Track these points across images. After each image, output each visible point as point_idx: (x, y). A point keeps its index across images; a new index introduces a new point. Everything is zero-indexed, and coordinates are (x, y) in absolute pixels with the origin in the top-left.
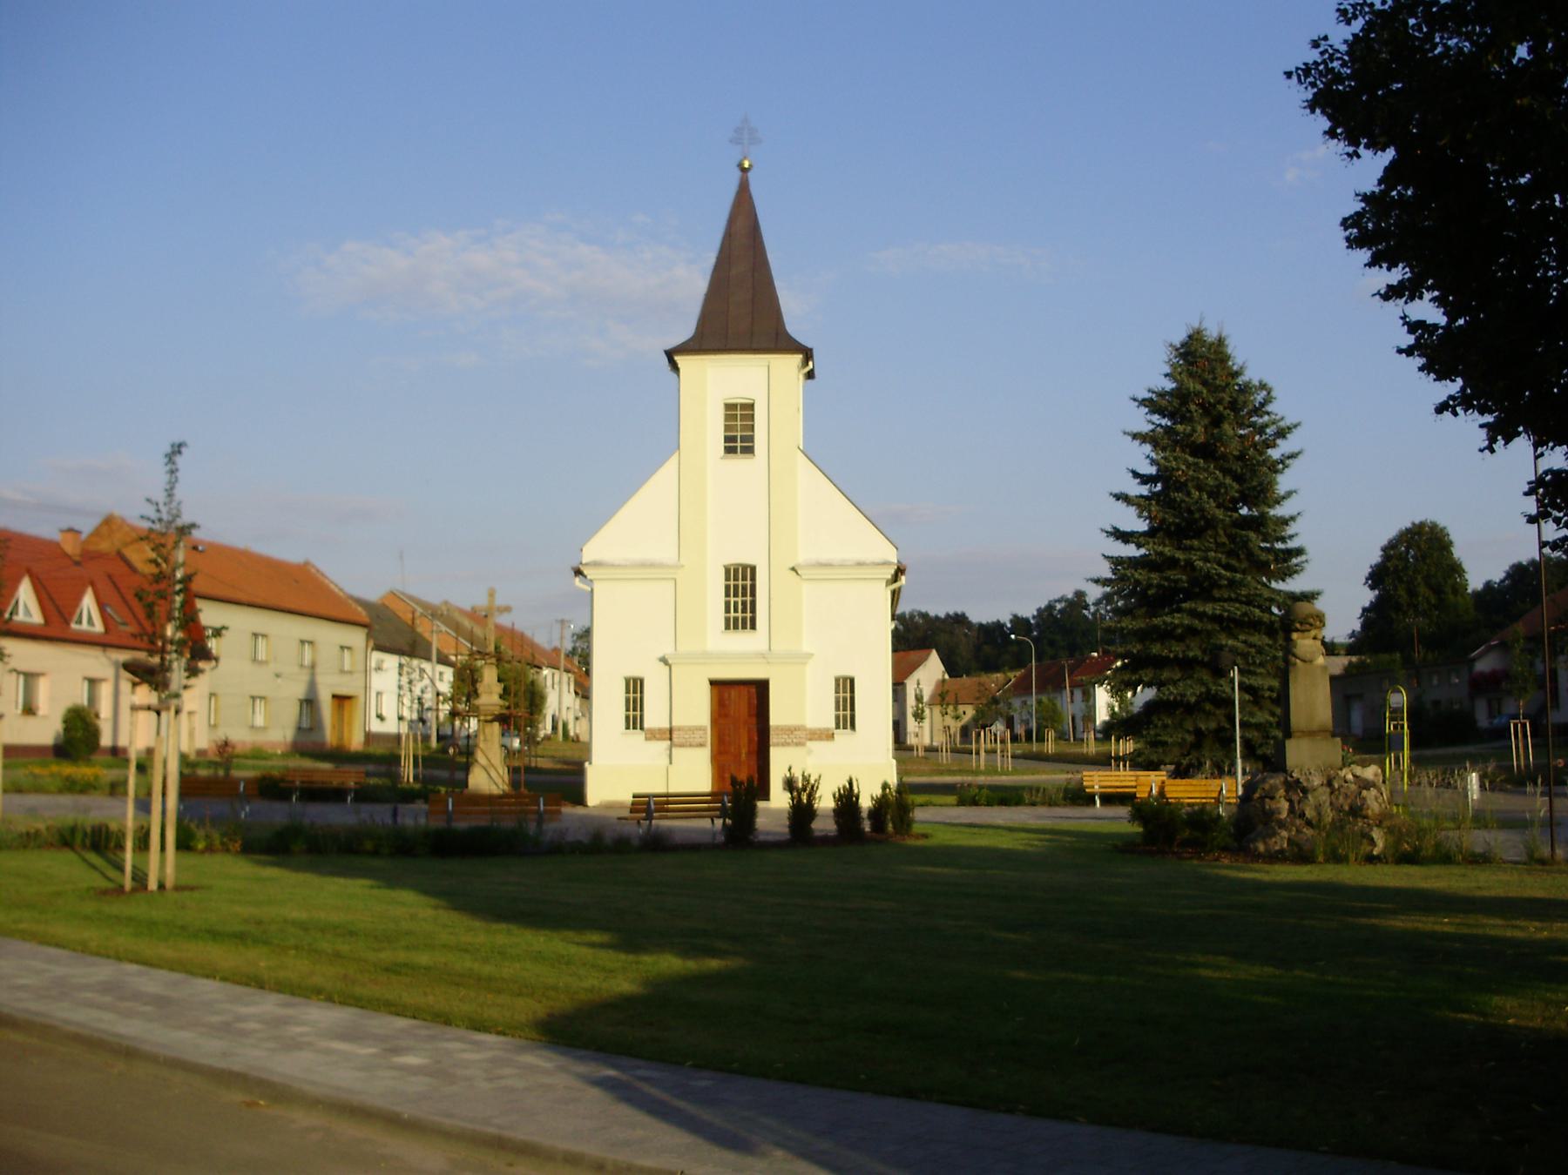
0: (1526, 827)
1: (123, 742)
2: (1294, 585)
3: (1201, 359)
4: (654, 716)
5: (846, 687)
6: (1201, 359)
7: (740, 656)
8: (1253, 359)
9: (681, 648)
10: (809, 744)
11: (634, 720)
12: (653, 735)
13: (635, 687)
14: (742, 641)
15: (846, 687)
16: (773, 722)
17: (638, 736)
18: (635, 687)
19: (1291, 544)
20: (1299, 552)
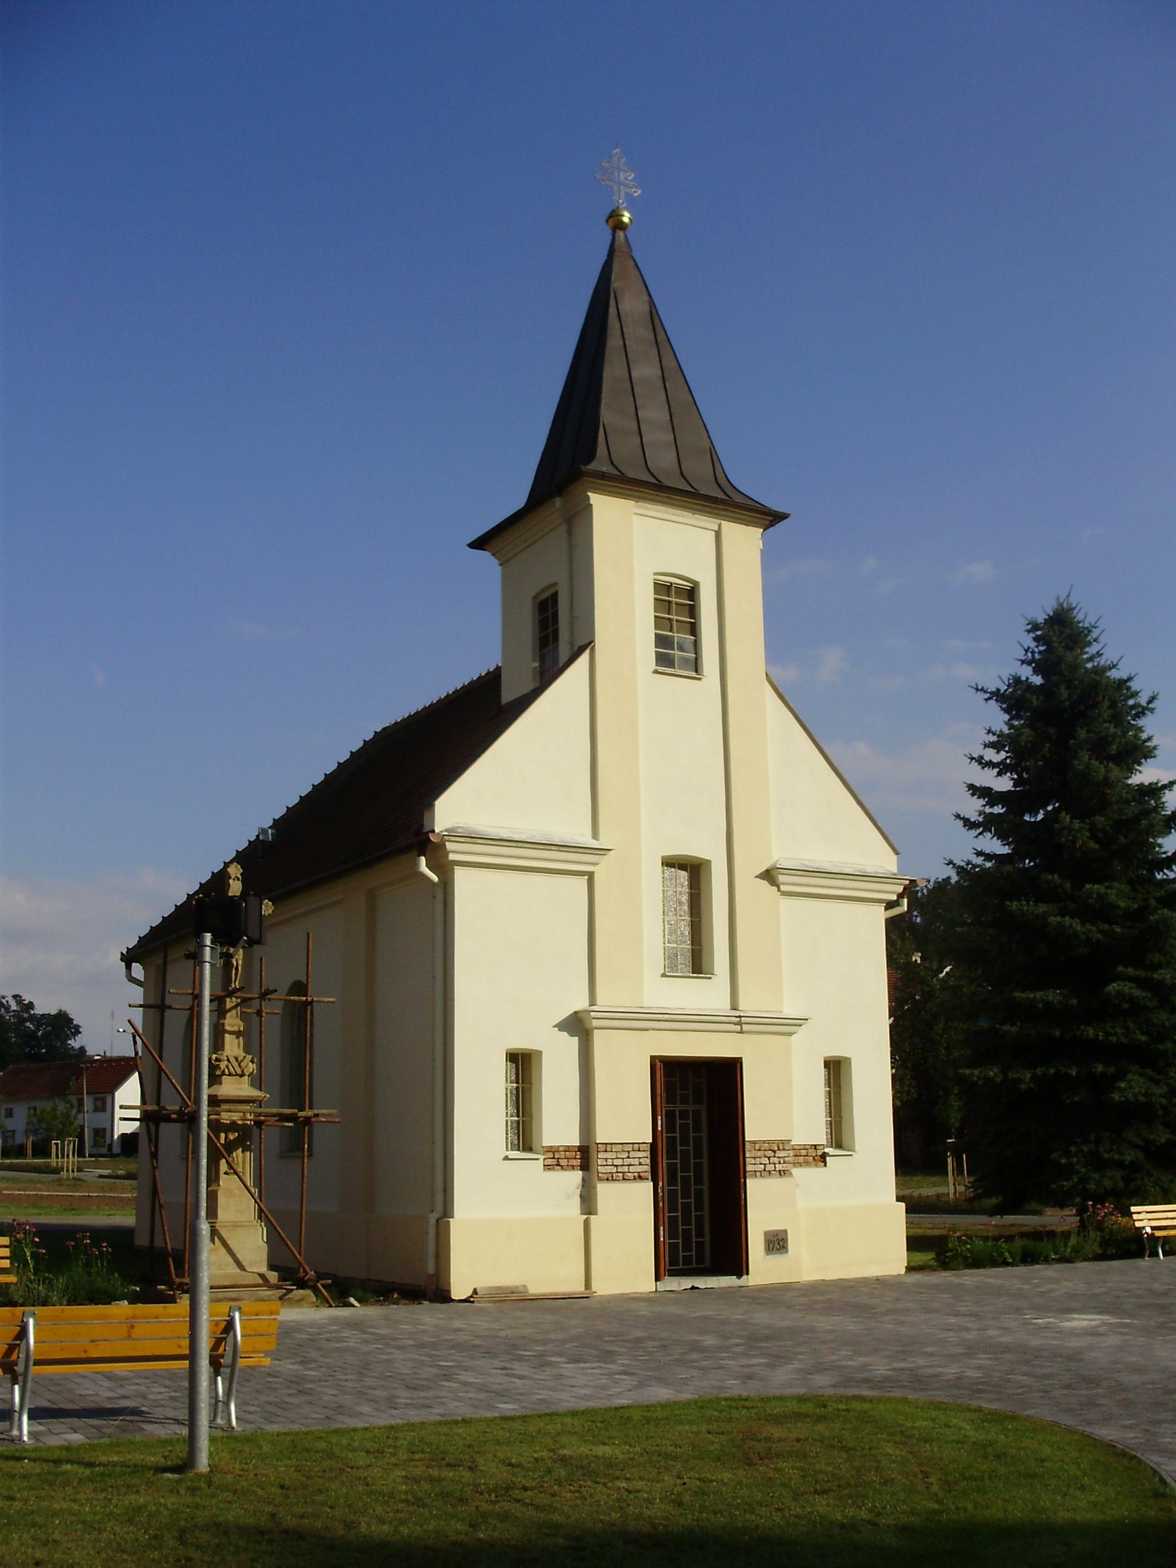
0: (1139, 1254)
1: (158, 1243)
2: (1026, 672)
3: (1060, 637)
4: (558, 1125)
5: (836, 1071)
6: (1060, 637)
7: (691, 1016)
8: (1085, 615)
9: (605, 1000)
10: (795, 1171)
11: (523, 1134)
12: (556, 1159)
13: (522, 1064)
14: (707, 996)
15: (836, 1071)
16: (749, 1136)
17: (532, 1168)
18: (522, 1064)
19: (1032, 635)
20: (1029, 631)
